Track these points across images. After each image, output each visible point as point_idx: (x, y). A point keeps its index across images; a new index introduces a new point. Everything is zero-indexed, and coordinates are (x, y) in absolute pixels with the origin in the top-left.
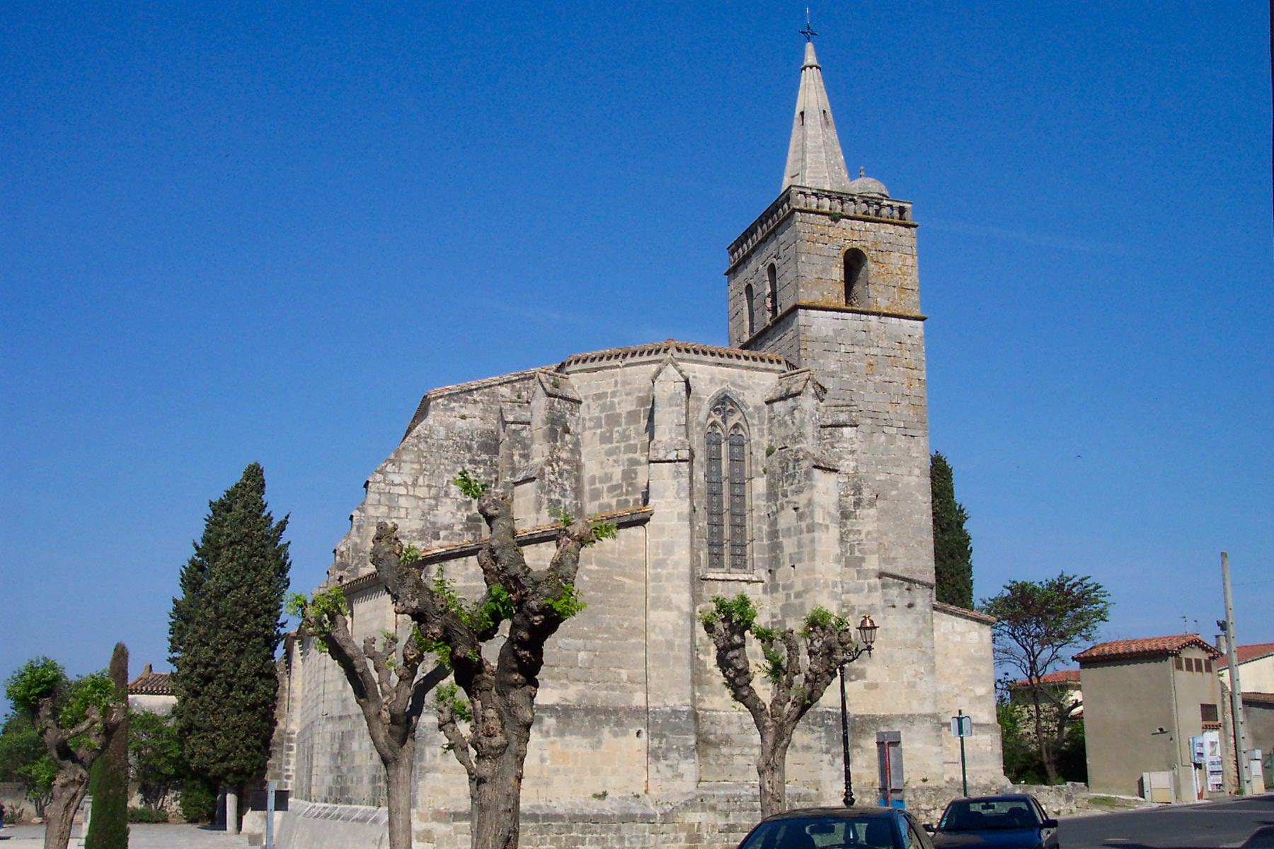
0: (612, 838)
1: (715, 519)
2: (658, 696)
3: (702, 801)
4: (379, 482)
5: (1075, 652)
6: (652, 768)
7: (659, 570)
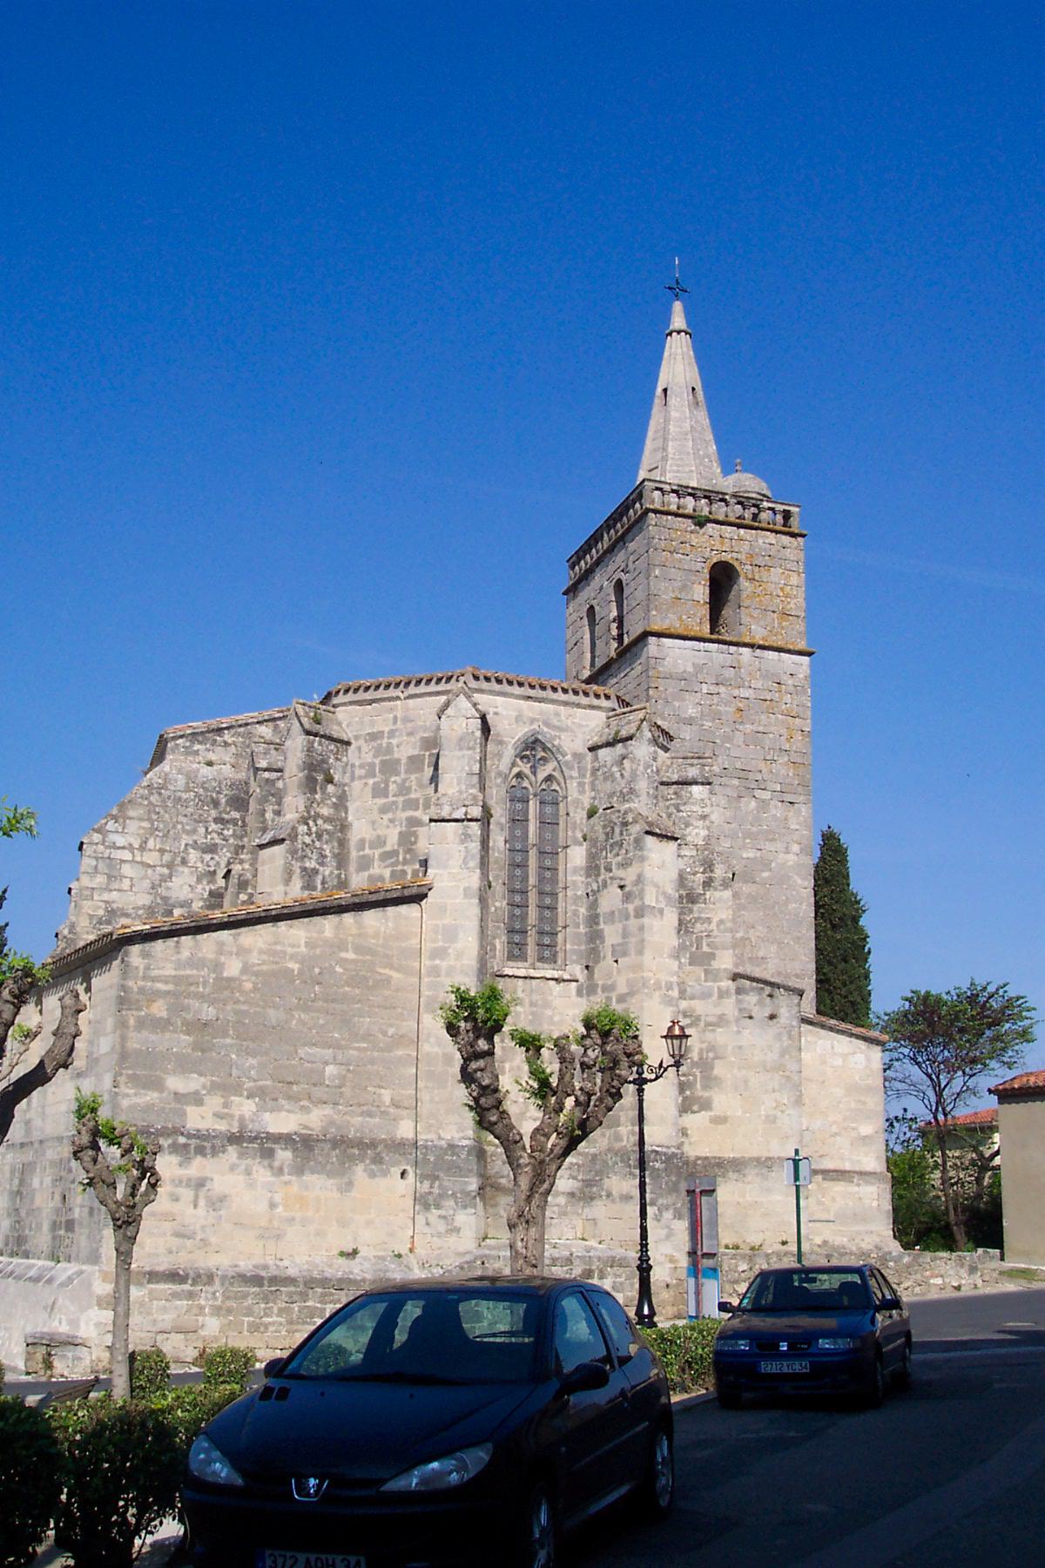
1: (518, 898)
2: (431, 1126)
3: (483, 1263)
4: (97, 844)
5: (993, 1082)
6: (420, 1219)
7: (438, 962)
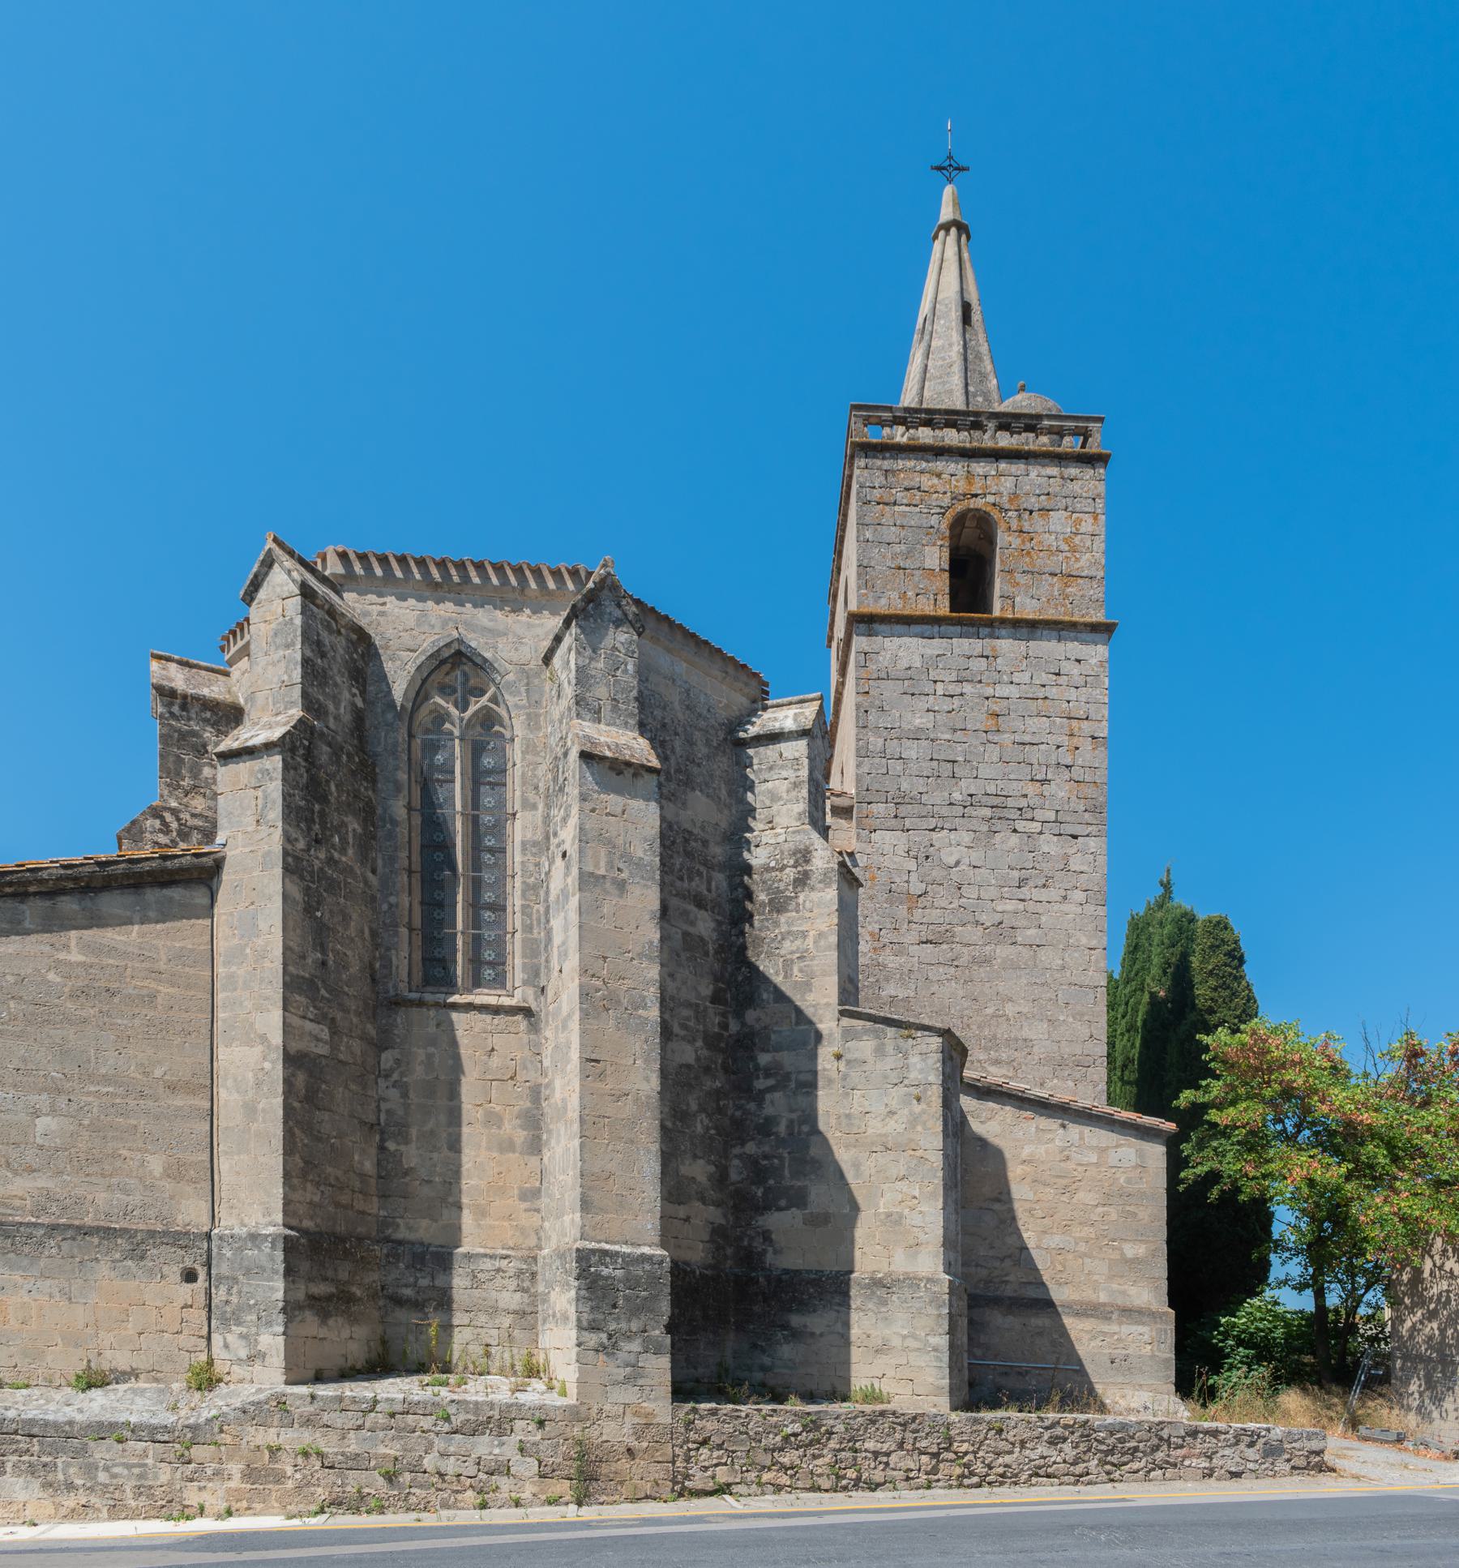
0: (67, 1465)
